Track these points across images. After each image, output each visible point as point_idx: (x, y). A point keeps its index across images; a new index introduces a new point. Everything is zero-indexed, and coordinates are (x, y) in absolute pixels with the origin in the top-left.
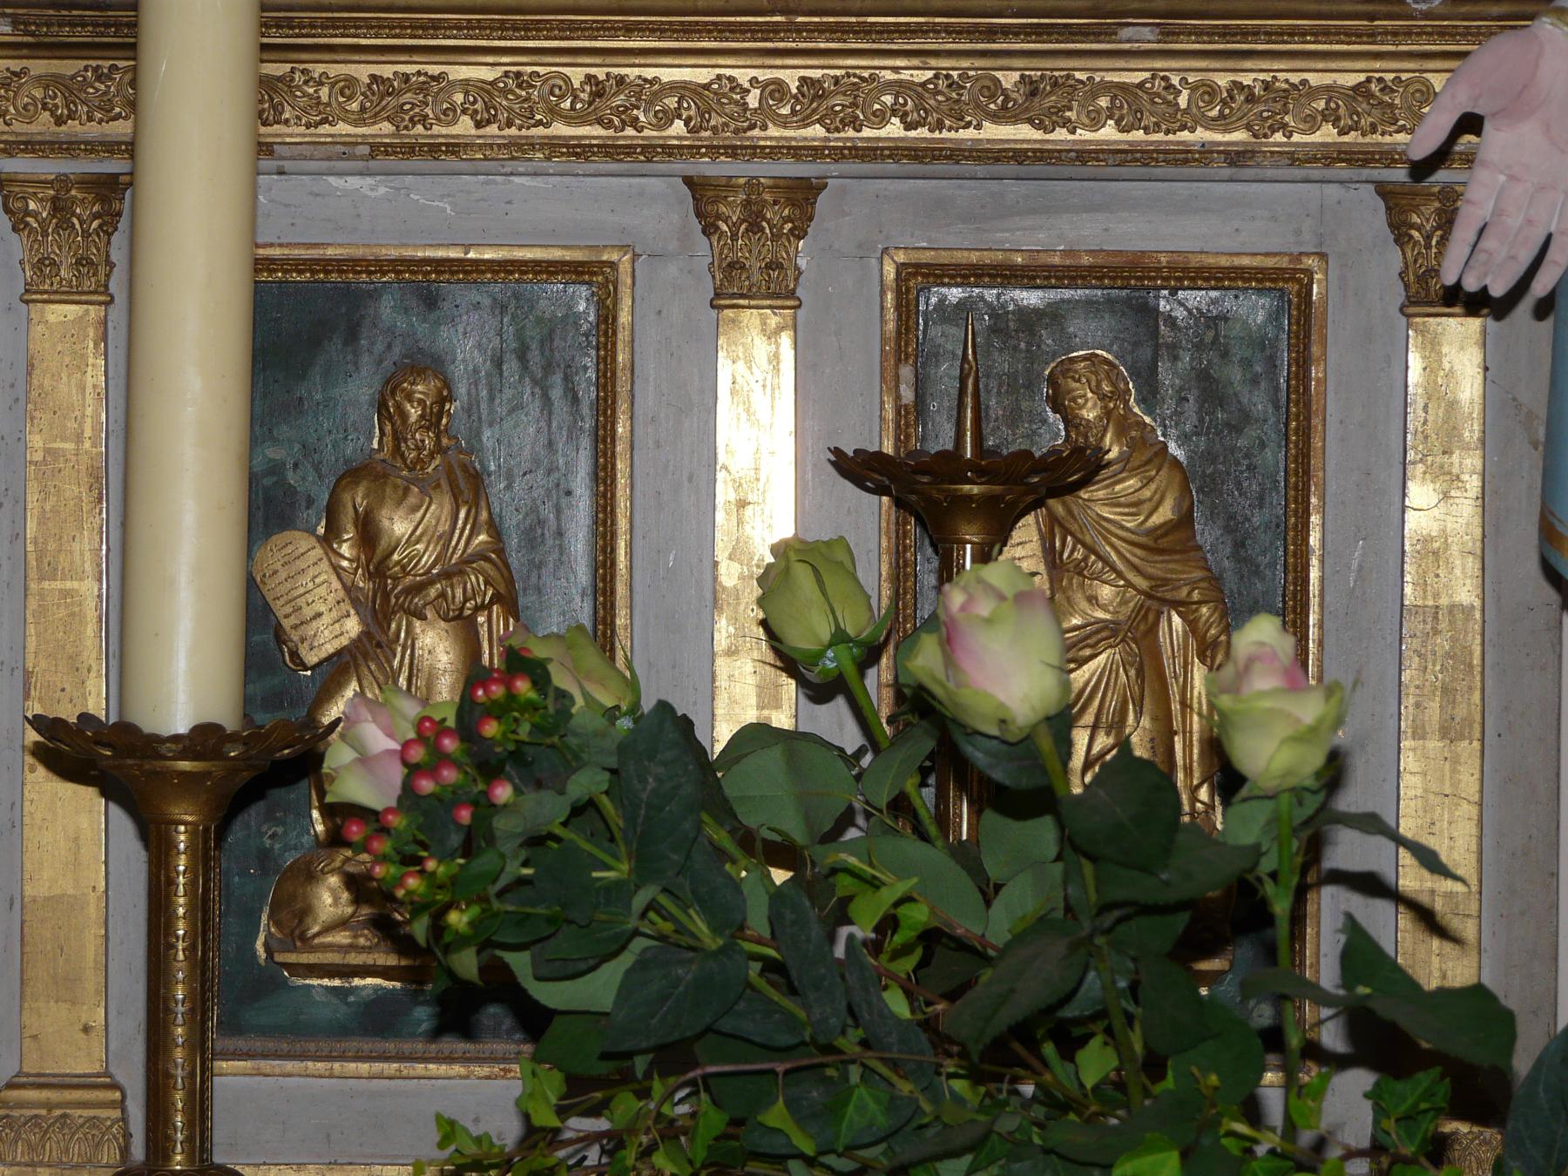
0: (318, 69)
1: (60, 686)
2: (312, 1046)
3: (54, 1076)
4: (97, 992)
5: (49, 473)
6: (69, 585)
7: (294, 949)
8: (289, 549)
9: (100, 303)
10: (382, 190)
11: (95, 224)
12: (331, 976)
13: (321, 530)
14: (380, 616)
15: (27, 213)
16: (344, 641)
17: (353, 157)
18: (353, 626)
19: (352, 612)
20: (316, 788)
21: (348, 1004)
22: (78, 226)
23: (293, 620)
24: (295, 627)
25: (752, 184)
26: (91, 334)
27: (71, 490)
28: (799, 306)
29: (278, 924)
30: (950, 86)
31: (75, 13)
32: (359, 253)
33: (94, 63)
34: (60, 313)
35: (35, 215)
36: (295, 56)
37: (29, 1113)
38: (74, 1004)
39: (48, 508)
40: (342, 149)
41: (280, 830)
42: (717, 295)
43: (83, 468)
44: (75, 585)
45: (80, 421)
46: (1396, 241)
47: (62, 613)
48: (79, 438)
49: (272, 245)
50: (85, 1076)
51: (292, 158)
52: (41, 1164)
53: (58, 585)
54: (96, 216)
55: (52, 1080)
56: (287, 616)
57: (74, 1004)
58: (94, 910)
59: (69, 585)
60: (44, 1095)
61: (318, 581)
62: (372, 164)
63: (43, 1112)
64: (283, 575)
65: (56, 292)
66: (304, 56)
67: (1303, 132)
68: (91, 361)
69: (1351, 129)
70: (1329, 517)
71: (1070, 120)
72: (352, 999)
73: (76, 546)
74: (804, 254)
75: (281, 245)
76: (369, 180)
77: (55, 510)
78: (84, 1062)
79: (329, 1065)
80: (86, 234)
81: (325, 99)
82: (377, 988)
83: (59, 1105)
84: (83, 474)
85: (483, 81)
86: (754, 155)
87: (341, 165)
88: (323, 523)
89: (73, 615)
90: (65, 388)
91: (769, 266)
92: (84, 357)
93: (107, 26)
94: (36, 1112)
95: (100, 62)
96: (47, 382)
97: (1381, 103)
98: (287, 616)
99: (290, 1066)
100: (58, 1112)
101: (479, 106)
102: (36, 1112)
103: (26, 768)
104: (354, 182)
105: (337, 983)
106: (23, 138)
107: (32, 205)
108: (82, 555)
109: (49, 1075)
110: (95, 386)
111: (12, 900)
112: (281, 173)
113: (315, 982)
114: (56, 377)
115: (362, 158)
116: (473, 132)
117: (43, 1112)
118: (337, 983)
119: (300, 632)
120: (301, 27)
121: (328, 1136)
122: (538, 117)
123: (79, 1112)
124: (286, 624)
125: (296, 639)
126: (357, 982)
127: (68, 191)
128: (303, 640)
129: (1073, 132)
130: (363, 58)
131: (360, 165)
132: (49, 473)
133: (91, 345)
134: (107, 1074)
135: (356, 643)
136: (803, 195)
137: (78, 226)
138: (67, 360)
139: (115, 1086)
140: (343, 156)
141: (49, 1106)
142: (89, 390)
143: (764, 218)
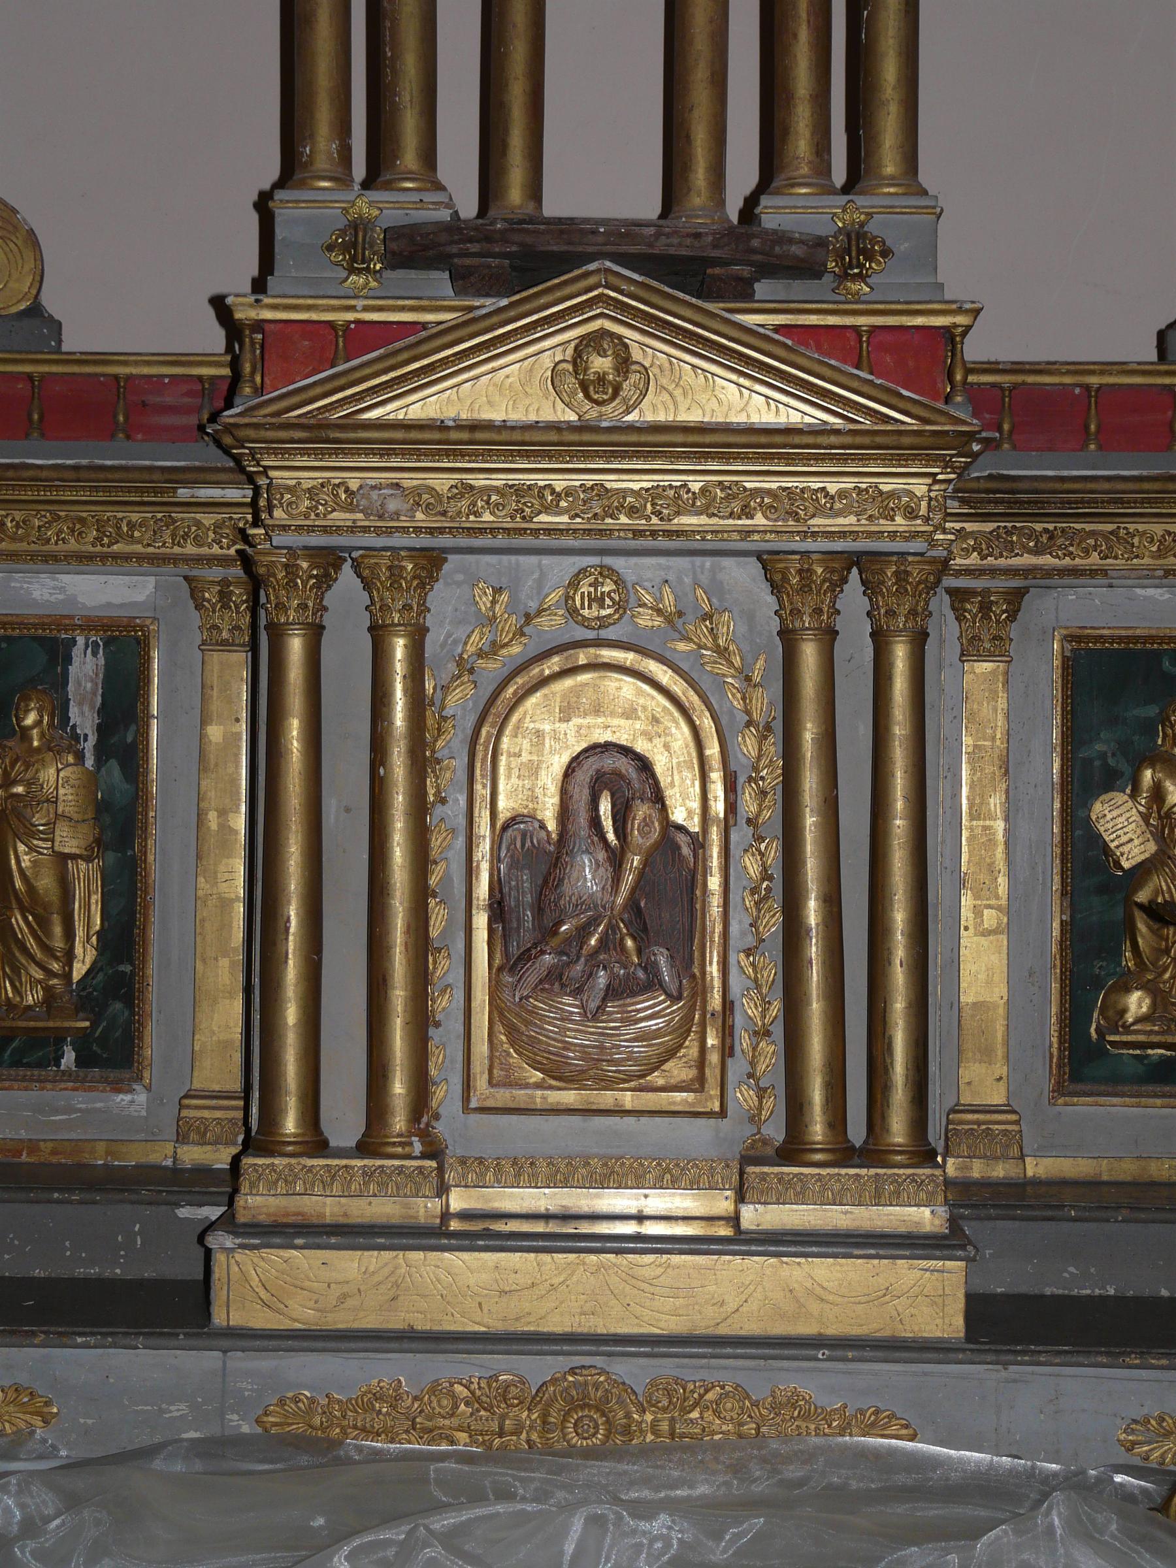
0: (1132, 528)
1: (982, 881)
2: (1126, 1089)
3: (979, 1105)
4: (1003, 1057)
5: (976, 759)
6: (988, 823)
7: (1117, 1033)
8: (1113, 802)
9: (1006, 662)
10: (1167, 596)
11: (1004, 616)
12: (1135, 1048)
13: (1128, 791)
14: (1168, 840)
15: (204, 599)
16: (1147, 855)
17: (1154, 577)
18: (1152, 847)
19: (1151, 839)
20: (1130, 940)
21: (1143, 1064)
22: (233, 608)
23: (1116, 843)
24: (1117, 847)
25: (986, 592)
26: (1001, 680)
27: (989, 769)
28: (1011, 661)
29: (1105, 1018)
30: (1006, 533)
31: (998, 496)
32: (1153, 632)
33: (1003, 524)
34: (985, 667)
35: (209, 601)
36: (1118, 520)
37: (967, 1127)
38: (990, 1064)
39: (975, 779)
40: (1147, 572)
41: (1104, 964)
42: (962, 655)
43: (996, 756)
44: (992, 823)
45: (994, 728)
46: (196, 608)
47: (984, 839)
48: (993, 739)
49: (1104, 628)
50: (996, 1105)
51: (1119, 578)
52: (974, 1157)
53: (981, 823)
54: (1004, 612)
55: (978, 1108)
56: (1112, 841)
57: (990, 1064)
58: (1001, 1011)
59: (988, 823)
60: (976, 1116)
61: (1130, 820)
62: (1164, 581)
63: (975, 1127)
64: (1109, 817)
65: (980, 656)
66: (1125, 520)
67: (1082, 558)
68: (1000, 695)
69: (988, 555)
70: (1050, 780)
71: (1072, 553)
72: (1146, 1062)
73: (992, 801)
74: (1014, 630)
75: (1109, 628)
76: (1159, 591)
77: (980, 780)
78: (997, 1097)
79: (1138, 1100)
80: (998, 622)
81: (1136, 544)
82: (1162, 1055)
83: (984, 1123)
84: (996, 759)
85: (985, 532)
86: (1015, 575)
87: (1146, 581)
88: (1130, 787)
89: (990, 840)
90: (986, 710)
91: (994, 638)
92: (996, 692)
93: (1015, 503)
94: (971, 1126)
95: (1007, 524)
96: (975, 706)
97: (1005, 540)
98: (1112, 841)
99: (1115, 1100)
100: (984, 1127)
101: (984, 546)
102: (971, 1126)
103: (962, 928)
104: (1151, 592)
105: (1138, 1052)
106: (964, 568)
107: (207, 595)
108: (995, 806)
109: (976, 1105)
110: (1003, 709)
111: (952, 1003)
112: (1111, 586)
113: (1125, 1051)
114: (980, 704)
115: (1160, 578)
116: (979, 562)
117: (975, 1127)
118: (1138, 1052)
119: (1121, 849)
120: (1129, 502)
121: (1136, 1142)
122: (1016, 551)
123: (996, 1126)
124: (1112, 845)
125: (1118, 854)
126: (1150, 1052)
127: (229, 587)
128: (1122, 854)
129: (1074, 559)
130: (1102, 520)
131: (1157, 581)
132: (976, 759)
133: (1001, 685)
134: (1008, 1105)
135: (1154, 856)
136: (1016, 598)
137: (233, 608)
138: (987, 694)
139: (1014, 1112)
140: (1147, 577)
141: (979, 1123)
142: (999, 711)
143: (992, 611)
